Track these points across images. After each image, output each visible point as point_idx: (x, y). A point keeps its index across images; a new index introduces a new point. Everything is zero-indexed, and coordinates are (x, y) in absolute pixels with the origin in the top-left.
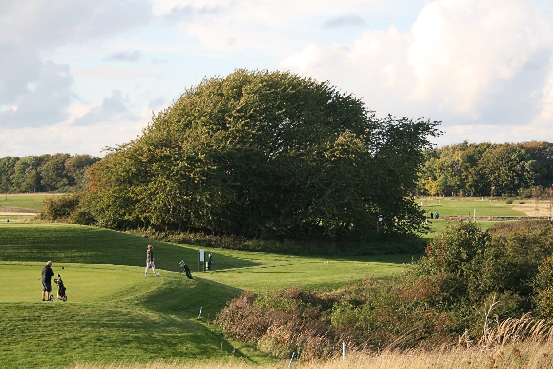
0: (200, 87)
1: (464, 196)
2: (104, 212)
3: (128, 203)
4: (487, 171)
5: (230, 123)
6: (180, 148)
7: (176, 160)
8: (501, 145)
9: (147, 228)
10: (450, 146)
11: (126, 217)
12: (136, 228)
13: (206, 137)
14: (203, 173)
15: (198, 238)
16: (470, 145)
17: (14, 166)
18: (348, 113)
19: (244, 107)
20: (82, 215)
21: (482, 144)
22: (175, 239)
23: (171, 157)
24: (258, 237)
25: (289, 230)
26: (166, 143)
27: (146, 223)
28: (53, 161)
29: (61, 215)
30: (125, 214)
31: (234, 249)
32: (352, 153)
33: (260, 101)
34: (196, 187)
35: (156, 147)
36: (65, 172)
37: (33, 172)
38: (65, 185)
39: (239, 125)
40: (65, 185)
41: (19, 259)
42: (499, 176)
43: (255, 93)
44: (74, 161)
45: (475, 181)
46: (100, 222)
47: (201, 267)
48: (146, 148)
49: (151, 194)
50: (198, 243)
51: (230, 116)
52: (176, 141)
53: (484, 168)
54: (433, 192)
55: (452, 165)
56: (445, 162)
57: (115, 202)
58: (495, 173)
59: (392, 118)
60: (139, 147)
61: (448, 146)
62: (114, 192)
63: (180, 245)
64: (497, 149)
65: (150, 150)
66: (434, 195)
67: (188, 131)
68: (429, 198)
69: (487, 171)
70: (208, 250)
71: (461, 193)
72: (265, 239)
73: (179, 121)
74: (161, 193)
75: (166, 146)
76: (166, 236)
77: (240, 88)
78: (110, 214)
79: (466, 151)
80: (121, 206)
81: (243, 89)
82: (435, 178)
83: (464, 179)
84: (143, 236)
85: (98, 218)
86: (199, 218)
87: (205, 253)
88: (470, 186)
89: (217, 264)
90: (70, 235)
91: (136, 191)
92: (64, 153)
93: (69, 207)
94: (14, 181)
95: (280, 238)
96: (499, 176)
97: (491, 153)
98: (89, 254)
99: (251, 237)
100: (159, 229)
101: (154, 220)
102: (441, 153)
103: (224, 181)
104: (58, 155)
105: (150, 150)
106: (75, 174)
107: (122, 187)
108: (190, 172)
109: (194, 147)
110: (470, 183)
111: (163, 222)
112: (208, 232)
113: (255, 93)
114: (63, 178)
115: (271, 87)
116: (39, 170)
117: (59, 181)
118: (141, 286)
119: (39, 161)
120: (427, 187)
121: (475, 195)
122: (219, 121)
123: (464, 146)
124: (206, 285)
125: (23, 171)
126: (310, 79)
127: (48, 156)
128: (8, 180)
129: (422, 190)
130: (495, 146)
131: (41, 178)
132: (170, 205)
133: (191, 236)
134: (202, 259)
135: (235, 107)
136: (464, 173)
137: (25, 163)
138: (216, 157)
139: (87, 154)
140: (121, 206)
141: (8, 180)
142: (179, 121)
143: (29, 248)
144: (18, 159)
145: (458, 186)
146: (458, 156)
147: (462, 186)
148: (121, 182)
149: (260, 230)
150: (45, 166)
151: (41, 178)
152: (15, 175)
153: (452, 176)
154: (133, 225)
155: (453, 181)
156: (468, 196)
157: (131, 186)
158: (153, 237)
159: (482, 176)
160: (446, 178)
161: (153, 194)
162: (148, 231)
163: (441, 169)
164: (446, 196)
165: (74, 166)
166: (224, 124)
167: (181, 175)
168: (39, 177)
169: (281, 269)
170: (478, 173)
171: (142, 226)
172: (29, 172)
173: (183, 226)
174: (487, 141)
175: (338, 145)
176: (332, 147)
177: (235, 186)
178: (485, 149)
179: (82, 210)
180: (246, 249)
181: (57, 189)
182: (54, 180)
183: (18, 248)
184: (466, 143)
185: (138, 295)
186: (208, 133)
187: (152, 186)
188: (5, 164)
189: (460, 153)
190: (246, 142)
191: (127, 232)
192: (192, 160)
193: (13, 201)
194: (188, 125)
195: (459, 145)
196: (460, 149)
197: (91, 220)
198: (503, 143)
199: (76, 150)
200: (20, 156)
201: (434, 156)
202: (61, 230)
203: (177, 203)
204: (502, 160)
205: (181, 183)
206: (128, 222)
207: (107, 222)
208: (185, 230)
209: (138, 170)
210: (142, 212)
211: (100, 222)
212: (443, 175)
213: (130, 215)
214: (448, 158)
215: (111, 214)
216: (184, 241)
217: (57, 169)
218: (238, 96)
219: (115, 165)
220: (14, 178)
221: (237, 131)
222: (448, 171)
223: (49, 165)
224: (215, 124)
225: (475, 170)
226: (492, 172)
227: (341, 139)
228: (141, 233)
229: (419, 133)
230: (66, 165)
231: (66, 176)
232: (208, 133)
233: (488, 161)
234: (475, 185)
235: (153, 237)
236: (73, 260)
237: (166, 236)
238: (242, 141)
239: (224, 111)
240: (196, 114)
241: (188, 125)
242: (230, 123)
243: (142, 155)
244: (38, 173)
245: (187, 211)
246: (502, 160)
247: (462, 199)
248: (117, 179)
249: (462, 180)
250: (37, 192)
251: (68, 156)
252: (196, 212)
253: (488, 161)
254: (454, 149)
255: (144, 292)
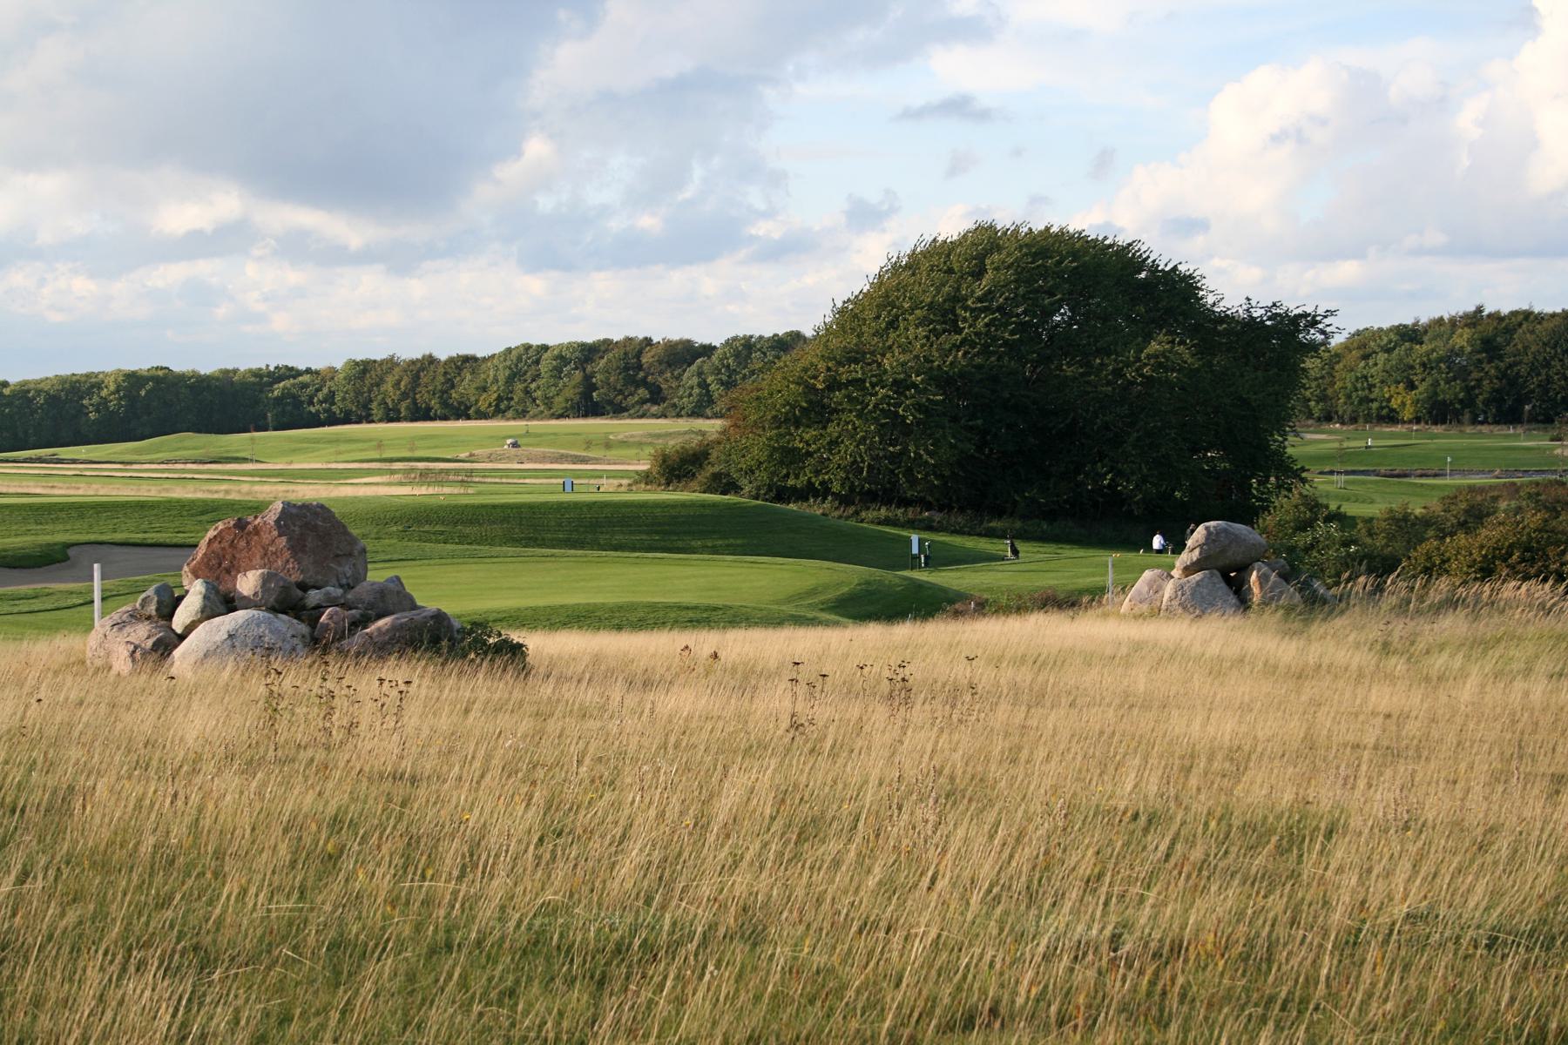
0: (913, 254)
1: (1474, 422)
2: (753, 472)
3: (790, 457)
4: (1524, 370)
5: (965, 320)
6: (879, 365)
7: (873, 385)
8: (1554, 315)
9: (825, 499)
10: (1446, 317)
11: (791, 482)
12: (807, 499)
13: (923, 346)
14: (919, 407)
15: (910, 515)
16: (1489, 316)
17: (537, 362)
18: (1172, 296)
19: (990, 292)
20: (716, 477)
21: (1514, 314)
22: (871, 519)
23: (864, 381)
24: (1011, 515)
25: (1066, 501)
26: (854, 356)
27: (823, 492)
28: (616, 353)
29: (679, 478)
30: (787, 476)
31: (970, 534)
32: (1173, 370)
33: (1016, 281)
34: (907, 431)
35: (840, 364)
36: (641, 374)
37: (578, 375)
38: (643, 402)
39: (980, 324)
40: (643, 402)
41: (634, 549)
42: (1549, 380)
43: (1008, 268)
44: (660, 350)
45: (1497, 391)
46: (747, 489)
47: (913, 563)
48: (822, 366)
49: (831, 443)
50: (912, 525)
51: (966, 308)
52: (873, 353)
53: (1515, 364)
54: (1407, 414)
55: (1448, 359)
56: (1433, 350)
57: (771, 456)
58: (1539, 374)
59: (1253, 303)
60: (812, 364)
61: (1441, 319)
62: (770, 439)
63: (880, 528)
64: (1545, 324)
65: (829, 369)
66: (1410, 422)
67: (892, 335)
68: (1399, 428)
69: (1524, 370)
70: (925, 535)
71: (1467, 416)
72: (1024, 517)
73: (878, 317)
74: (845, 444)
75: (856, 361)
76: (857, 513)
77: (981, 257)
78: (762, 476)
79: (1479, 328)
80: (781, 463)
81: (988, 261)
82: (1411, 386)
83: (1473, 388)
84: (819, 512)
85: (743, 482)
86: (913, 482)
87: (921, 542)
88: (1487, 403)
89: (936, 560)
90: (708, 512)
91: (807, 437)
92: (641, 337)
93: (693, 463)
94: (539, 393)
95: (1050, 515)
96: (1549, 380)
97: (1532, 332)
98: (739, 542)
99: (999, 513)
100: (845, 501)
101: (836, 487)
102: (1426, 332)
103: (955, 419)
104: (629, 340)
105: (829, 369)
106: (665, 380)
107: (782, 430)
108: (898, 405)
109: (903, 364)
110: (1486, 395)
111: (852, 489)
112: (929, 507)
113: (1008, 268)
114: (637, 387)
115: (1035, 256)
116: (589, 368)
117: (632, 394)
118: (826, 587)
119: (589, 353)
120: (1394, 404)
121: (1497, 422)
122: (944, 316)
123: (1475, 319)
124: (919, 586)
125: (557, 372)
126: (1106, 238)
127: (608, 342)
128: (527, 392)
129: (1385, 412)
130: (1540, 318)
131: (594, 387)
132: (863, 461)
133: (900, 512)
134: (915, 550)
135: (973, 292)
136: (1475, 375)
137: (561, 357)
138: (943, 381)
139: (686, 336)
140: (781, 463)
141: (527, 392)
142: (878, 317)
143: (647, 533)
144: (545, 348)
145: (1461, 402)
146: (1462, 339)
147: (1468, 402)
148: (777, 422)
149: (1015, 503)
150: (603, 362)
151: (594, 387)
152: (541, 382)
153: (1448, 382)
154: (802, 495)
155: (1451, 392)
156: (1482, 423)
157: (797, 428)
158: (836, 514)
159: (1510, 381)
160: (1436, 384)
161: (834, 443)
162: (827, 505)
163: (1424, 365)
164: (1435, 423)
165: (660, 362)
166: (955, 322)
167: (882, 410)
168: (589, 386)
169: (1042, 566)
170: (1503, 375)
171: (816, 497)
172: (569, 375)
173: (884, 494)
174: (1525, 307)
175: (1149, 357)
176: (1138, 359)
177: (971, 428)
178: (1520, 325)
179: (716, 469)
180: (990, 534)
181: (626, 410)
182: (621, 392)
183: (631, 533)
184: (1479, 310)
185: (822, 598)
186: (927, 338)
187: (833, 429)
188: (519, 359)
189: (1467, 333)
190: (993, 353)
191: (792, 506)
192: (901, 386)
193: (540, 435)
194: (892, 324)
195: (1466, 316)
196: (1466, 325)
197: (731, 487)
198: (1559, 310)
199: (664, 328)
200: (550, 344)
201: (1411, 340)
202: (684, 504)
203: (876, 458)
204: (1554, 347)
205: (883, 425)
206: (794, 488)
207: (758, 488)
208: (887, 502)
209: (810, 402)
210: (817, 473)
211: (747, 489)
212: (1429, 380)
213: (797, 477)
214: (1439, 343)
215: (765, 475)
216: (887, 522)
217: (626, 369)
218: (979, 273)
219: (771, 395)
220: (539, 389)
221: (976, 334)
222: (1440, 372)
223: (609, 361)
224: (938, 322)
225: (1497, 368)
226: (1533, 369)
227: (1154, 347)
228: (815, 508)
229: (1299, 332)
230: (644, 361)
231: (644, 383)
232: (927, 338)
233: (1526, 348)
234: (1496, 398)
235: (836, 514)
236: (715, 551)
237: (857, 513)
238: (985, 351)
239: (956, 299)
240: (906, 306)
241: (892, 324)
242: (965, 320)
243: (815, 377)
244: (587, 378)
245: (892, 471)
246: (1554, 347)
247: (1469, 429)
248: (775, 417)
249: (1468, 390)
250: (585, 416)
251: (648, 341)
252: (909, 472)
253: (1526, 348)
254: (1453, 322)
255: (831, 595)
